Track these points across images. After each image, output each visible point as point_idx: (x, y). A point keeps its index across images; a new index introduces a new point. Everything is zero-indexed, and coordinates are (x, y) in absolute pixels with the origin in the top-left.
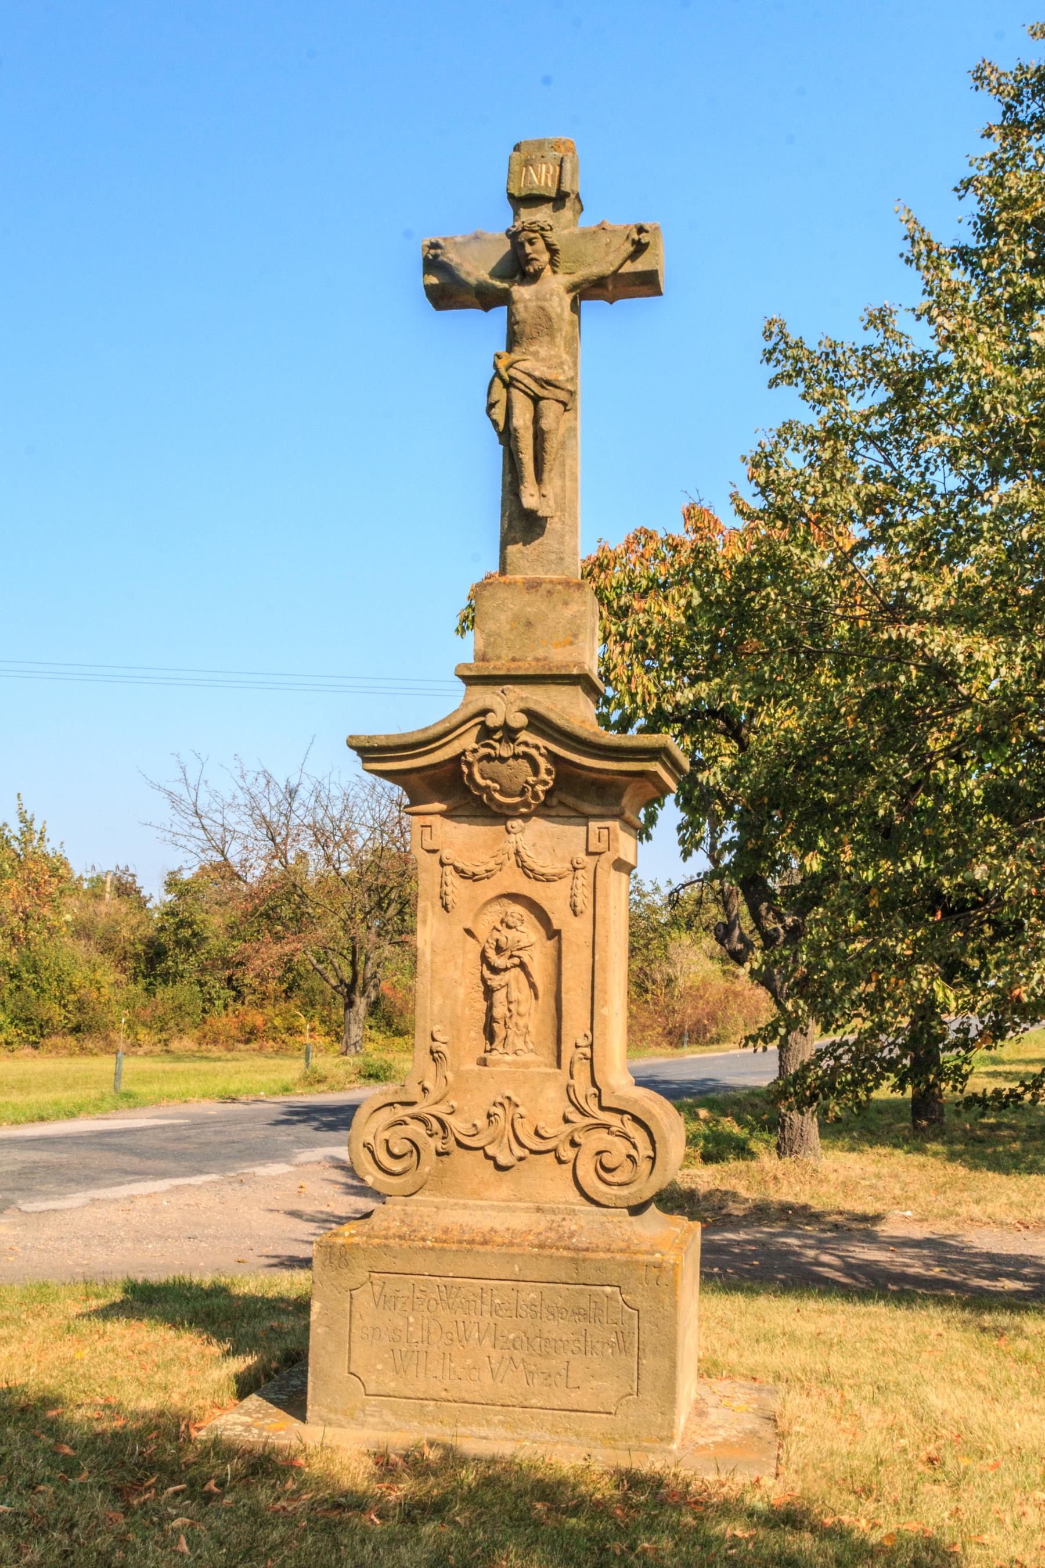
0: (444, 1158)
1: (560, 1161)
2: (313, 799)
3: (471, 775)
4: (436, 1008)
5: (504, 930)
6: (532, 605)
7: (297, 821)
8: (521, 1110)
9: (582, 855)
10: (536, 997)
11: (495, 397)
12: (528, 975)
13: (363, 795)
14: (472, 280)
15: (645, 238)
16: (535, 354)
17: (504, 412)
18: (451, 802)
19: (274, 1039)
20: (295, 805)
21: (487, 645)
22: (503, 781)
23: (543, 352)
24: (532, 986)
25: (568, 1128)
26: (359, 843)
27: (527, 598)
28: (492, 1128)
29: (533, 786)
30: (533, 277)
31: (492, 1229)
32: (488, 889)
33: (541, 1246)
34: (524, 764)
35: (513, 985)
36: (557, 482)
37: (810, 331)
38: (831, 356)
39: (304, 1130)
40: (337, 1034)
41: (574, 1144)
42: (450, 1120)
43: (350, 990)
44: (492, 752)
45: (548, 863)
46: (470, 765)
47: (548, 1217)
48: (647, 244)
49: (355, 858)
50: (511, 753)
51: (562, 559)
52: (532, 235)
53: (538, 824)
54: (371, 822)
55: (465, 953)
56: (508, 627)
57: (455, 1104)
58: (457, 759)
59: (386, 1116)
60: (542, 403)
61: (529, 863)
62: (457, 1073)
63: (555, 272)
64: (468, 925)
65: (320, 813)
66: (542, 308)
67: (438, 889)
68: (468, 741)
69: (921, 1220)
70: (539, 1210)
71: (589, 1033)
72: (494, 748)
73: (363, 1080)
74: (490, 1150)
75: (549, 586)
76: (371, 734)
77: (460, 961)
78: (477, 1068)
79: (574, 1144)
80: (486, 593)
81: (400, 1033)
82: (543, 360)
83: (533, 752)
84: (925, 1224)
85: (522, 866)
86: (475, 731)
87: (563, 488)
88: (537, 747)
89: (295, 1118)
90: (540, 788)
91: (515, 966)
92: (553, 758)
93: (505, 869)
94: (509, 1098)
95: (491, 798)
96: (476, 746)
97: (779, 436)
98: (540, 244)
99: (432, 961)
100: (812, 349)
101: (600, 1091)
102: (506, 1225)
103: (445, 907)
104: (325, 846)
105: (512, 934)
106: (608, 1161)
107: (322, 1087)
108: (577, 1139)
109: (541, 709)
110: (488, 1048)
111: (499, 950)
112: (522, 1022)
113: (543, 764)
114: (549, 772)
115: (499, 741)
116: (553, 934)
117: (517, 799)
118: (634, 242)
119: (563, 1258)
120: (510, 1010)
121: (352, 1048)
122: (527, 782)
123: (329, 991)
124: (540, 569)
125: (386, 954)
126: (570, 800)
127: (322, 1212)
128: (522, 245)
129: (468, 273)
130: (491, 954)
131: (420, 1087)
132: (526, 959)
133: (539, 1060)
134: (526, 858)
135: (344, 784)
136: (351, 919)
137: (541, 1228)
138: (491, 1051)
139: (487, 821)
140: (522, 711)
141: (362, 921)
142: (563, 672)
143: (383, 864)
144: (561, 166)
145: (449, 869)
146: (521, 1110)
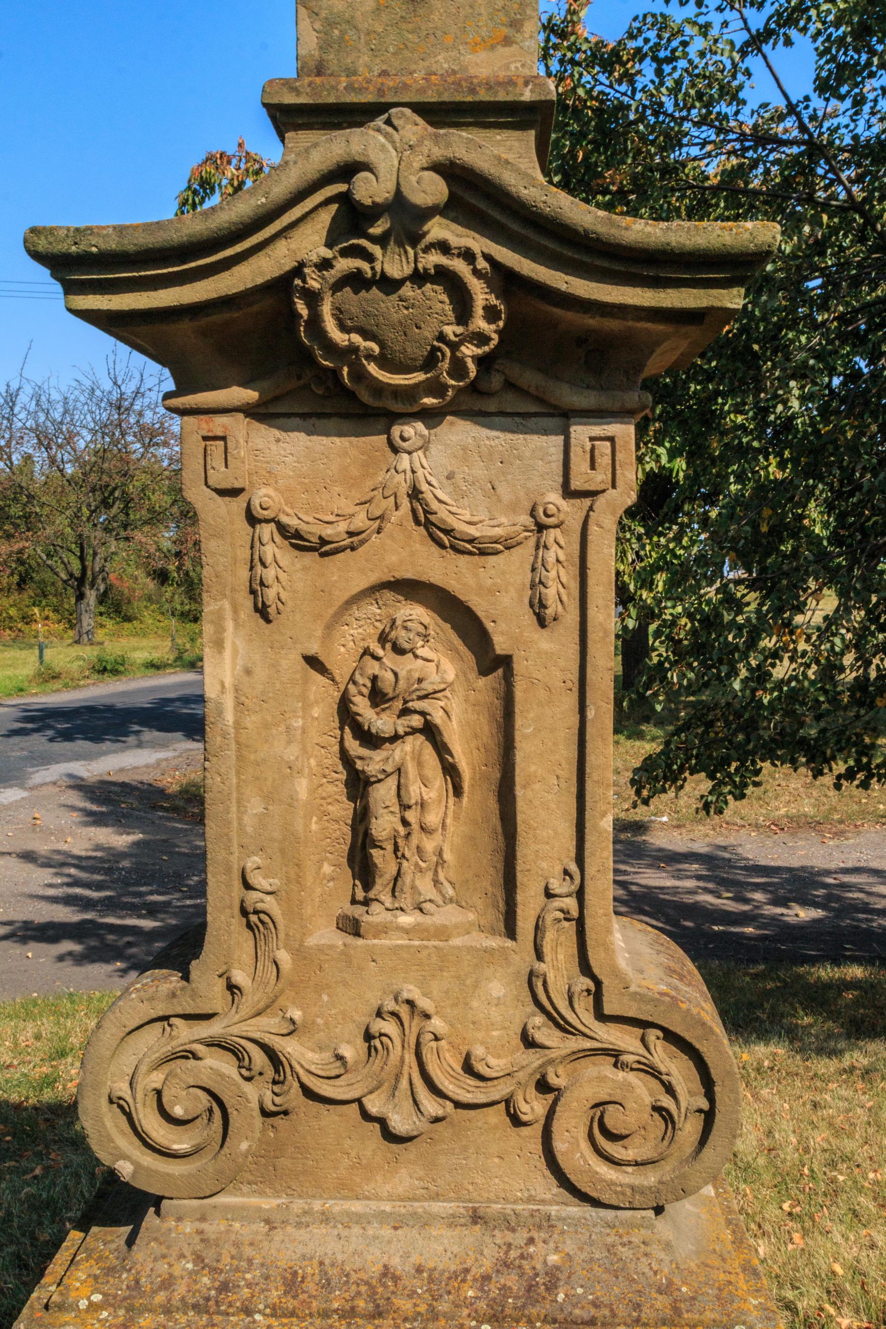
0: (278, 1121)
1: (516, 1121)
2: (34, 403)
3: (315, 320)
4: (248, 821)
5: (389, 659)
7: (20, 424)
8: (437, 1024)
9: (554, 497)
10: (458, 791)
12: (441, 749)
18: (266, 384)
19: (11, 628)
20: (17, 409)
21: (325, 45)
22: (389, 335)
24: (450, 771)
25: (533, 1059)
28: (377, 1062)
29: (454, 347)
31: (386, 1272)
32: (352, 573)
34: (437, 297)
35: (411, 769)
39: (38, 742)
40: (70, 621)
41: (543, 1086)
42: (289, 1048)
43: (80, 583)
45: (482, 515)
46: (313, 298)
50: (408, 270)
53: (459, 432)
54: (92, 425)
55: (307, 707)
57: (297, 1014)
58: (283, 286)
59: (151, 1041)
61: (442, 514)
62: (299, 953)
64: (314, 648)
65: (42, 417)
67: (245, 574)
68: (310, 242)
69: (678, 827)
70: (476, 1218)
71: (573, 868)
72: (370, 258)
73: (96, 676)
74: (374, 1106)
77: (299, 723)
78: (339, 940)
79: (543, 1086)
81: (128, 619)
83: (460, 266)
84: (683, 830)
85: (426, 521)
86: (326, 217)
88: (468, 256)
89: (30, 726)
90: (469, 351)
91: (414, 731)
92: (504, 280)
93: (388, 527)
94: (410, 1003)
95: (360, 375)
96: (328, 253)
99: (238, 725)
101: (598, 983)
102: (415, 1259)
103: (262, 611)
104: (48, 448)
105: (407, 666)
106: (614, 1119)
107: (57, 685)
108: (553, 1080)
110: (360, 895)
111: (377, 697)
112: (429, 845)
113: (481, 295)
114: (491, 314)
115: (382, 240)
116: (492, 662)
117: (419, 377)
120: (405, 823)
121: (85, 636)
122: (441, 337)
123: (60, 584)
125: (113, 549)
126: (530, 379)
127: (58, 852)
130: (361, 705)
131: (222, 982)
132: (438, 717)
133: (464, 922)
134: (434, 505)
136: (78, 517)
137: (487, 1264)
138: (366, 902)
139: (346, 425)
140: (437, 168)
141: (88, 519)
142: (501, 96)
143: (106, 465)
145: (267, 531)
146: (437, 1024)
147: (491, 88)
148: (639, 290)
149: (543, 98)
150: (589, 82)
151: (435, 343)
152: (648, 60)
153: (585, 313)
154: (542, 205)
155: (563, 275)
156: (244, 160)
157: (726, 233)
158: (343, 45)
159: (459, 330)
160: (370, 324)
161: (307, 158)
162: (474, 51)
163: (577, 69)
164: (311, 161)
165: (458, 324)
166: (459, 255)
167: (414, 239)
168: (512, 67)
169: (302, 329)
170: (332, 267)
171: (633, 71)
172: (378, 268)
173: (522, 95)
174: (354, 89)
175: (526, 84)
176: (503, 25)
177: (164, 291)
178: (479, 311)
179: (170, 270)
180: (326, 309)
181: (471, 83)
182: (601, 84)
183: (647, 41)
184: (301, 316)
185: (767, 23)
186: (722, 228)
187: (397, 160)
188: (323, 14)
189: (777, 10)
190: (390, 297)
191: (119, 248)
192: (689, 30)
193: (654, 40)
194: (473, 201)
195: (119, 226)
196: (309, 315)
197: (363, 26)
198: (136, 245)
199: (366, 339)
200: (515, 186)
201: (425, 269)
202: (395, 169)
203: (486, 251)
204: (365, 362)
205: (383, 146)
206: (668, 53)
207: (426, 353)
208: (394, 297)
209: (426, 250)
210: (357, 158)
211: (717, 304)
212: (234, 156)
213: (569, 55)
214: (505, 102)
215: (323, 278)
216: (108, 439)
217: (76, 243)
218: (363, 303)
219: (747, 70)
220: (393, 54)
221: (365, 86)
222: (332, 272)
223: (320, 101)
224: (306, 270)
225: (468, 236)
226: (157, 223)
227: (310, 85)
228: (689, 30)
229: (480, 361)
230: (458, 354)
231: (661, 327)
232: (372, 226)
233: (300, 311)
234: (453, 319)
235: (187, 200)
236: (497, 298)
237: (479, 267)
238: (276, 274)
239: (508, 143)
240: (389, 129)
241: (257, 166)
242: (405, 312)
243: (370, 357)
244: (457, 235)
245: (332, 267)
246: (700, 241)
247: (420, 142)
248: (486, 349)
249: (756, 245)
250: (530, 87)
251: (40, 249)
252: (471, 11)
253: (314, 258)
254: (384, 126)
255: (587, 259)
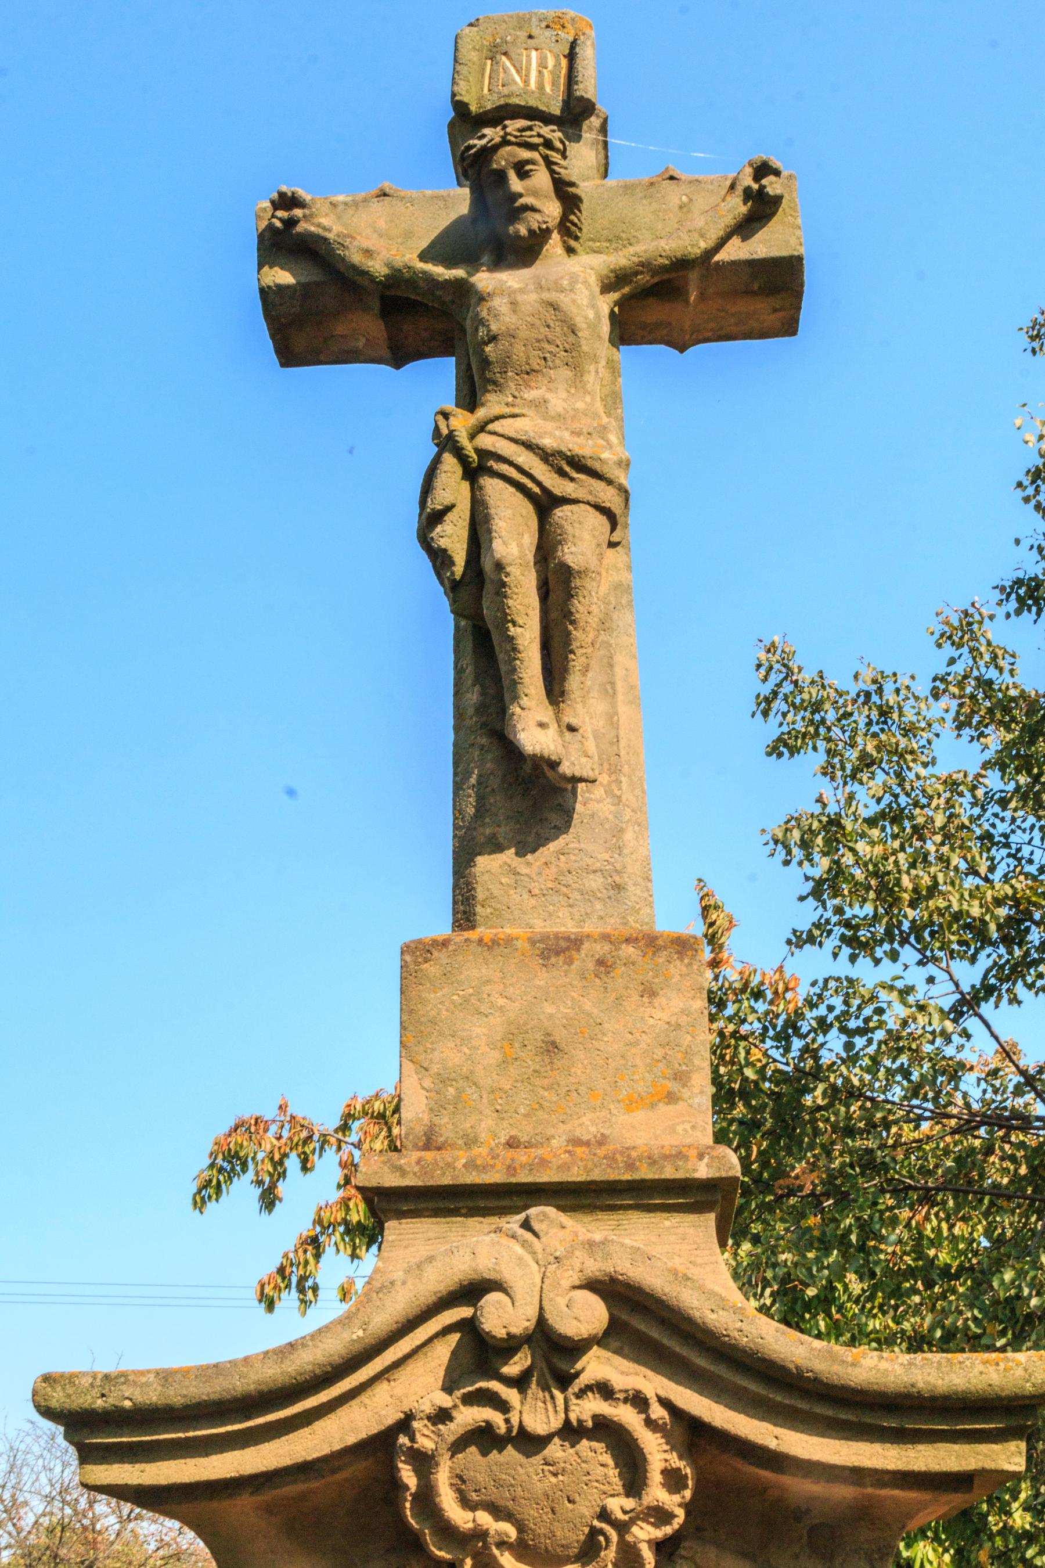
3: (426, 1497)
6: (562, 999)
11: (441, 497)
13: (36, 1449)
14: (378, 268)
15: (772, 186)
16: (541, 405)
17: (465, 534)
22: (530, 1513)
23: (557, 402)
26: (28, 1520)
27: (542, 978)
29: (622, 1528)
30: (525, 252)
34: (596, 1458)
36: (598, 705)
37: (835, 662)
38: (875, 698)
44: (497, 1418)
46: (424, 1462)
48: (777, 200)
49: (20, 1543)
50: (556, 1423)
51: (618, 887)
52: (525, 154)
54: (48, 1489)
56: (495, 1056)
58: (382, 1446)
60: (561, 513)
63: (570, 251)
66: (555, 307)
68: (419, 1385)
72: (503, 1406)
75: (602, 949)
76: (107, 1366)
80: (430, 969)
82: (559, 417)
83: (627, 1416)
86: (443, 1351)
87: (612, 717)
88: (639, 1401)
92: (691, 1434)
96: (445, 1401)
97: (776, 842)
98: (541, 178)
100: (841, 688)
109: (653, 1278)
114: (673, 1480)
115: (520, 1383)
118: (748, 194)
122: (604, 1515)
124: (563, 913)
128: (501, 177)
129: (368, 253)
135: (12, 1434)
140: (593, 1285)
142: (669, 1173)
144: (571, 56)
147: (655, 1162)
148: (877, 1447)
149: (724, 1174)
150: (760, 1061)
151: (596, 1523)
152: (834, 1032)
153: (805, 1476)
154: (736, 1334)
155: (771, 1427)
156: (287, 1126)
157: (992, 1369)
158: (459, 1106)
159: (630, 1503)
160: (503, 1498)
161: (420, 1277)
162: (629, 1109)
163: (743, 1044)
164: (424, 1280)
165: (628, 1496)
166: (626, 1400)
167: (564, 1381)
168: (680, 1129)
169: (408, 1505)
170: (451, 1419)
171: (815, 1046)
172: (515, 1421)
173: (695, 1170)
174: (476, 1167)
175: (701, 1156)
176: (665, 1078)
177: (219, 1456)
178: (655, 1477)
179: (229, 1428)
180: (443, 1478)
181: (629, 1156)
182: (775, 1061)
183: (831, 1009)
184: (407, 1488)
185: (985, 976)
186: (985, 1362)
187: (540, 1272)
188: (435, 1068)
189: (995, 963)
190: (531, 1460)
191: (162, 1401)
192: (883, 995)
193: (840, 1008)
194: (642, 1327)
195: (164, 1371)
196: (418, 1486)
197: (486, 1082)
198: (185, 1396)
199: (497, 1518)
200: (698, 1310)
201: (580, 1421)
202: (538, 1288)
203: (663, 1394)
204: (496, 1552)
205: (520, 1259)
206: (860, 1023)
207: (582, 1538)
208: (537, 1459)
209: (581, 1394)
210: (486, 1276)
211: (990, 1465)
212: (274, 1121)
213: (731, 1027)
214: (674, 1180)
215: (439, 1435)
216: (68, 1511)
217: (103, 1395)
218: (494, 1468)
219: (965, 1031)
220: (526, 1116)
221: (491, 1162)
222: (452, 1426)
223: (431, 1183)
224: (415, 1424)
225: (637, 1374)
226: (216, 1366)
227: (418, 1163)
228: (883, 995)
229: (660, 1547)
230: (629, 1538)
231: (913, 1495)
232: (506, 1364)
233: (406, 1480)
234: (620, 1489)
235: (211, 1181)
236: (680, 1458)
237: (653, 1416)
238: (375, 1429)
239: (680, 1230)
240: (528, 1236)
241: (304, 1134)
242: (553, 1480)
243: (502, 1544)
244: (622, 1373)
245: (451, 1419)
246: (957, 1381)
247: (570, 1253)
248: (668, 1530)
249: (1034, 1385)
250: (706, 1160)
251: (54, 1404)
252: (623, 1062)
253: (428, 1409)
254: (521, 1232)
255: (802, 1405)
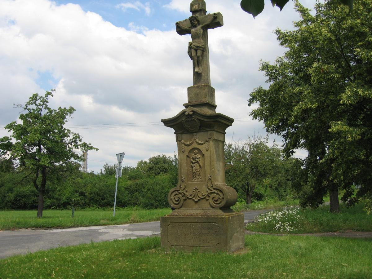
33: (201, 216)
35: (196, 166)
42: (186, 193)
47: (204, 211)
70: (203, 210)
92: (200, 120)
98: (195, 20)
119: (205, 218)
137: (203, 213)
